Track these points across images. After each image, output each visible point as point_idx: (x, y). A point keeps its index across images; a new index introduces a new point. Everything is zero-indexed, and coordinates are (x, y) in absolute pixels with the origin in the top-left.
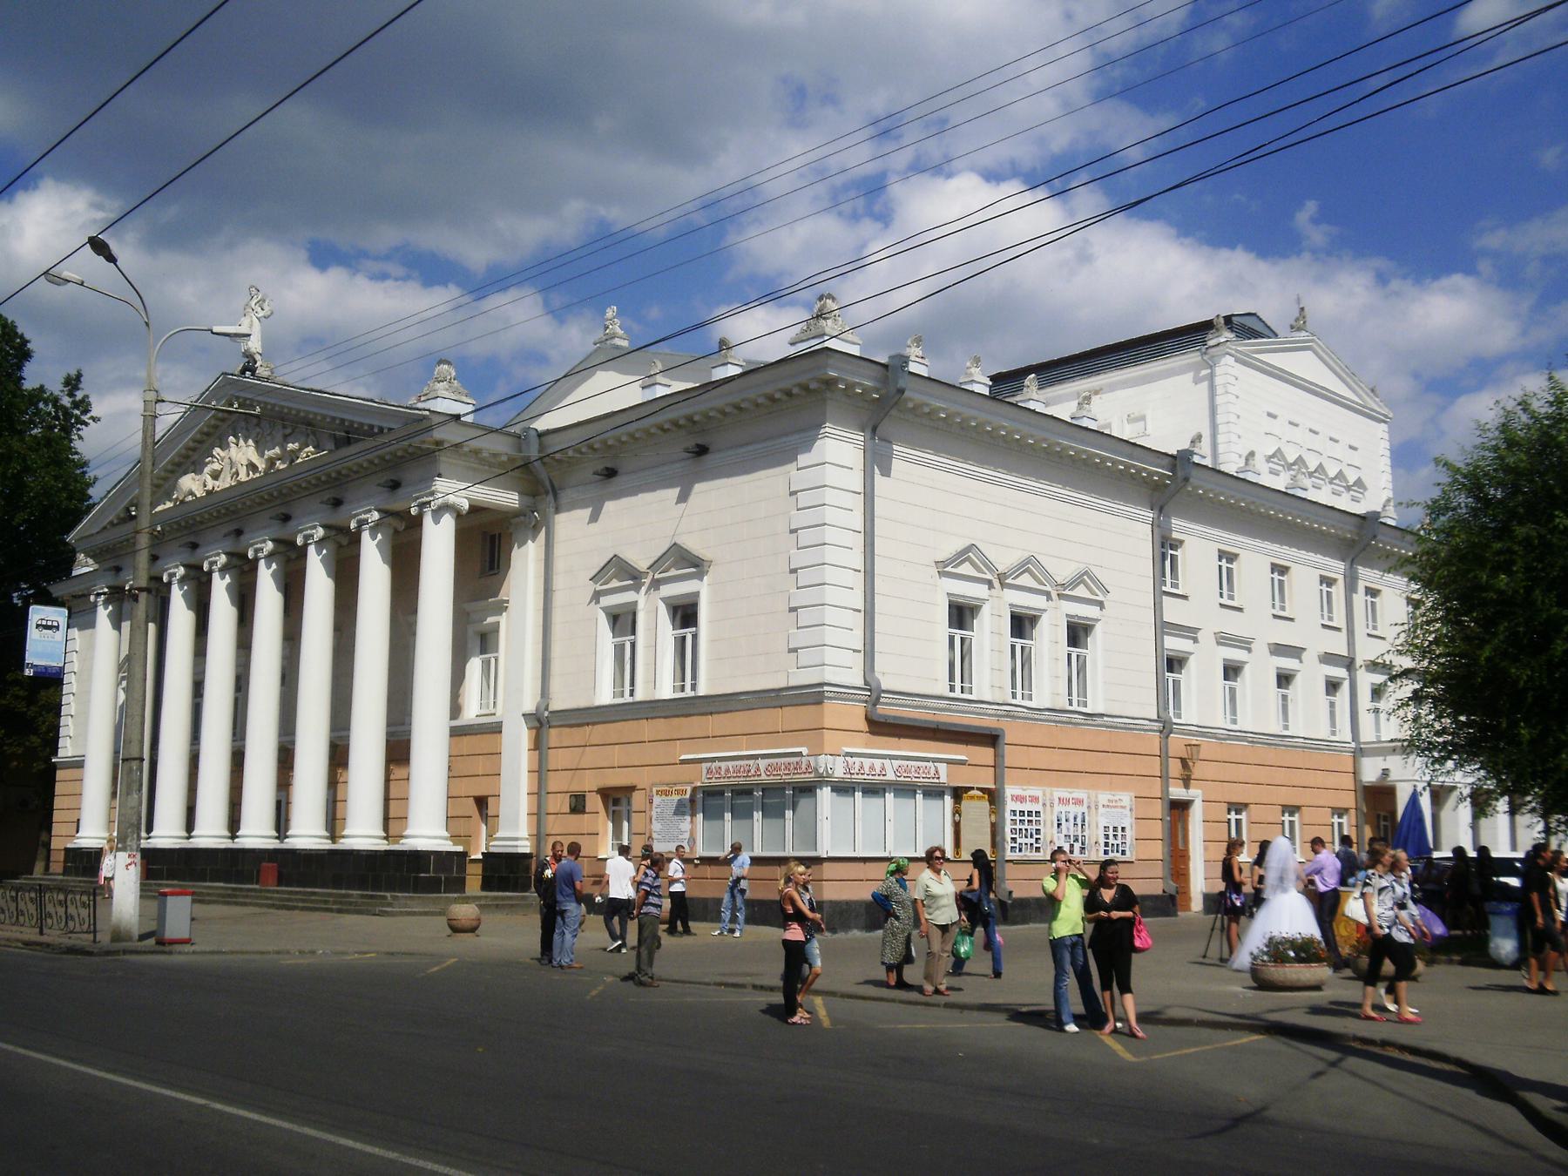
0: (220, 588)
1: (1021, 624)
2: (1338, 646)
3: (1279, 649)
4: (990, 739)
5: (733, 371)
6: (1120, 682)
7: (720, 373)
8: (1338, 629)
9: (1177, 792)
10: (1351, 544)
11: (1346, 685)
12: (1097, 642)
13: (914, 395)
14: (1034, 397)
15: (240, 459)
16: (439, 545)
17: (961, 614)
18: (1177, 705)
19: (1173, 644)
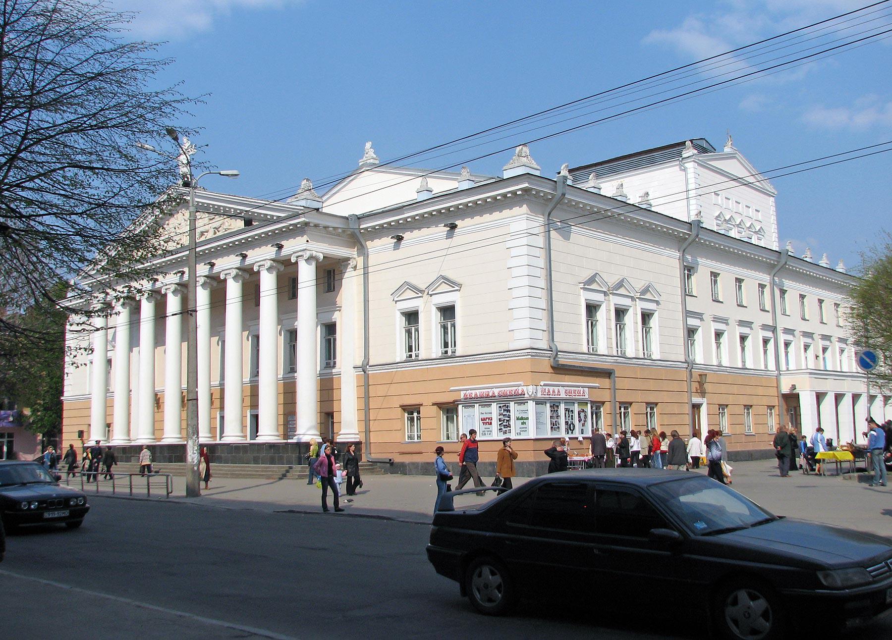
0: (147, 309)
1: (620, 313)
2: (768, 320)
3: (742, 323)
4: (607, 374)
6: (665, 343)
9: (696, 400)
11: (772, 340)
12: (654, 322)
13: (703, 236)
14: (590, 183)
17: (592, 309)
19: (692, 322)
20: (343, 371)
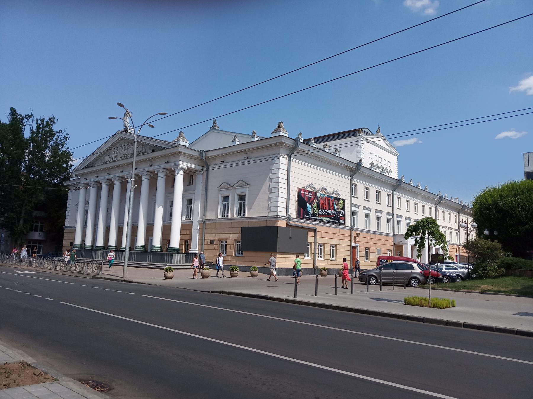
0: (131, 187)
2: (390, 210)
3: (377, 211)
5: (256, 139)
7: (253, 140)
8: (390, 207)
9: (354, 244)
10: (393, 186)
15: (309, 189)
16: (180, 179)
18: (354, 224)
19: (354, 209)
20: (323, 184)
